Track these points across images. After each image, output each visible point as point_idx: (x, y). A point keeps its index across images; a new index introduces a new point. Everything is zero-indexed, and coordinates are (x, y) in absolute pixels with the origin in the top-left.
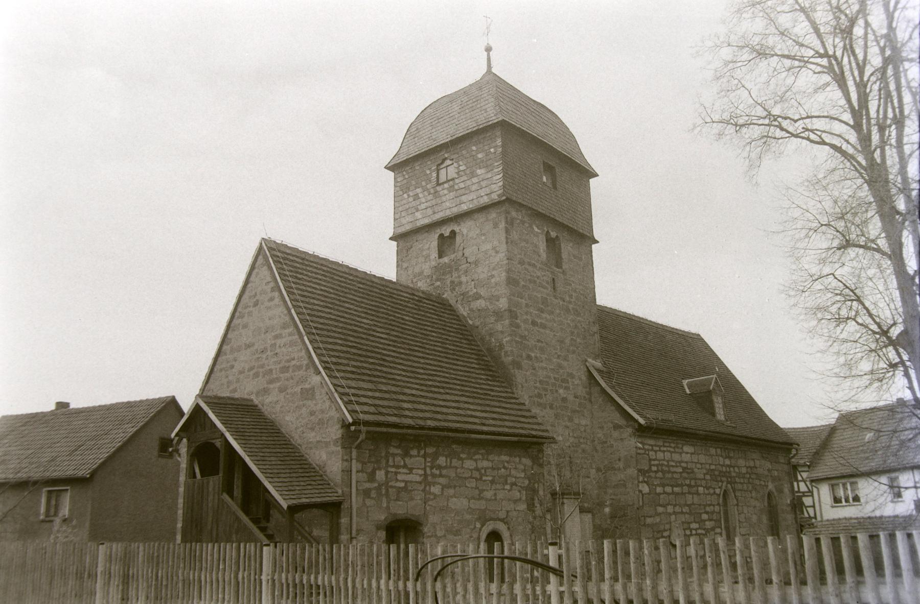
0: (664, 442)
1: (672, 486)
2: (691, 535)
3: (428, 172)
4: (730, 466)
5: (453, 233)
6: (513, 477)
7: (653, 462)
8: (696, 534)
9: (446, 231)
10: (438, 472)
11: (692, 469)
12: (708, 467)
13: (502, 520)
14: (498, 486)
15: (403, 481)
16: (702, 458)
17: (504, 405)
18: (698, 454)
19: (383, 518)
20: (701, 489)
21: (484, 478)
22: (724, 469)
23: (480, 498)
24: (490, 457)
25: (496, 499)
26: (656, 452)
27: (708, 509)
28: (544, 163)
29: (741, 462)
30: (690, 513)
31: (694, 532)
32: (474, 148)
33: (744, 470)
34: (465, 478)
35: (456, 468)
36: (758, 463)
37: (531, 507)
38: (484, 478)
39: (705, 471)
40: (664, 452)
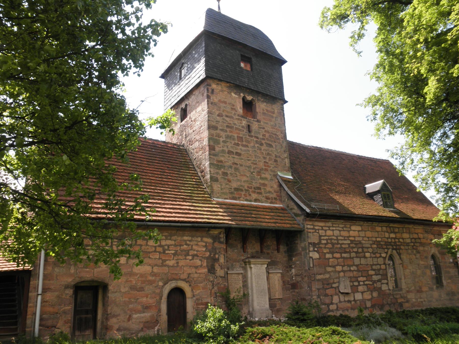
0: (202, 237)
1: (341, 253)
2: (359, 285)
4: (395, 238)
5: (186, 105)
6: (194, 250)
7: (322, 238)
8: (364, 285)
9: (183, 106)
11: (360, 241)
12: (374, 239)
13: (184, 280)
14: (180, 257)
16: (369, 234)
17: (194, 204)
18: (365, 231)
20: (368, 255)
21: (167, 252)
22: (390, 240)
23: (163, 265)
24: (174, 238)
25: (178, 266)
26: (326, 230)
27: (374, 267)
28: (241, 55)
29: (406, 236)
30: (358, 271)
31: (361, 283)
33: (409, 241)
34: (149, 252)
35: (141, 245)
36: (421, 236)
37: (212, 270)
38: (167, 252)
39: (371, 242)
40: (333, 230)
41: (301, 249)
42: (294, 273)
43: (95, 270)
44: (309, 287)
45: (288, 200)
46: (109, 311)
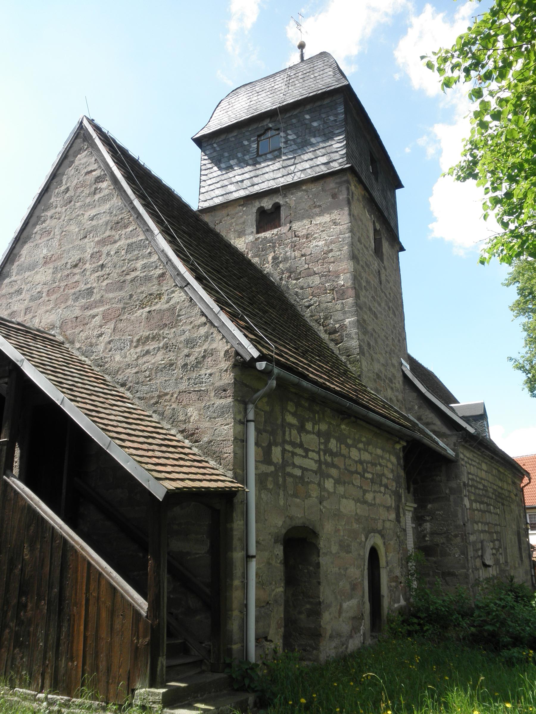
3: (246, 143)
5: (277, 207)
10: (329, 459)
15: (301, 467)
19: (280, 523)
32: (307, 117)
41: (447, 491)
42: (428, 530)
43: (306, 501)
44: (463, 553)
45: (419, 407)
46: (321, 596)
